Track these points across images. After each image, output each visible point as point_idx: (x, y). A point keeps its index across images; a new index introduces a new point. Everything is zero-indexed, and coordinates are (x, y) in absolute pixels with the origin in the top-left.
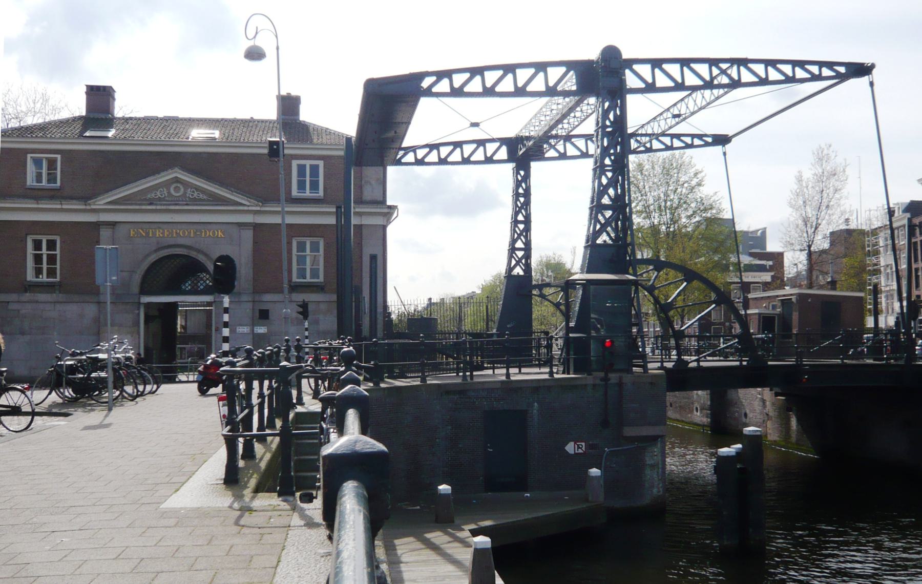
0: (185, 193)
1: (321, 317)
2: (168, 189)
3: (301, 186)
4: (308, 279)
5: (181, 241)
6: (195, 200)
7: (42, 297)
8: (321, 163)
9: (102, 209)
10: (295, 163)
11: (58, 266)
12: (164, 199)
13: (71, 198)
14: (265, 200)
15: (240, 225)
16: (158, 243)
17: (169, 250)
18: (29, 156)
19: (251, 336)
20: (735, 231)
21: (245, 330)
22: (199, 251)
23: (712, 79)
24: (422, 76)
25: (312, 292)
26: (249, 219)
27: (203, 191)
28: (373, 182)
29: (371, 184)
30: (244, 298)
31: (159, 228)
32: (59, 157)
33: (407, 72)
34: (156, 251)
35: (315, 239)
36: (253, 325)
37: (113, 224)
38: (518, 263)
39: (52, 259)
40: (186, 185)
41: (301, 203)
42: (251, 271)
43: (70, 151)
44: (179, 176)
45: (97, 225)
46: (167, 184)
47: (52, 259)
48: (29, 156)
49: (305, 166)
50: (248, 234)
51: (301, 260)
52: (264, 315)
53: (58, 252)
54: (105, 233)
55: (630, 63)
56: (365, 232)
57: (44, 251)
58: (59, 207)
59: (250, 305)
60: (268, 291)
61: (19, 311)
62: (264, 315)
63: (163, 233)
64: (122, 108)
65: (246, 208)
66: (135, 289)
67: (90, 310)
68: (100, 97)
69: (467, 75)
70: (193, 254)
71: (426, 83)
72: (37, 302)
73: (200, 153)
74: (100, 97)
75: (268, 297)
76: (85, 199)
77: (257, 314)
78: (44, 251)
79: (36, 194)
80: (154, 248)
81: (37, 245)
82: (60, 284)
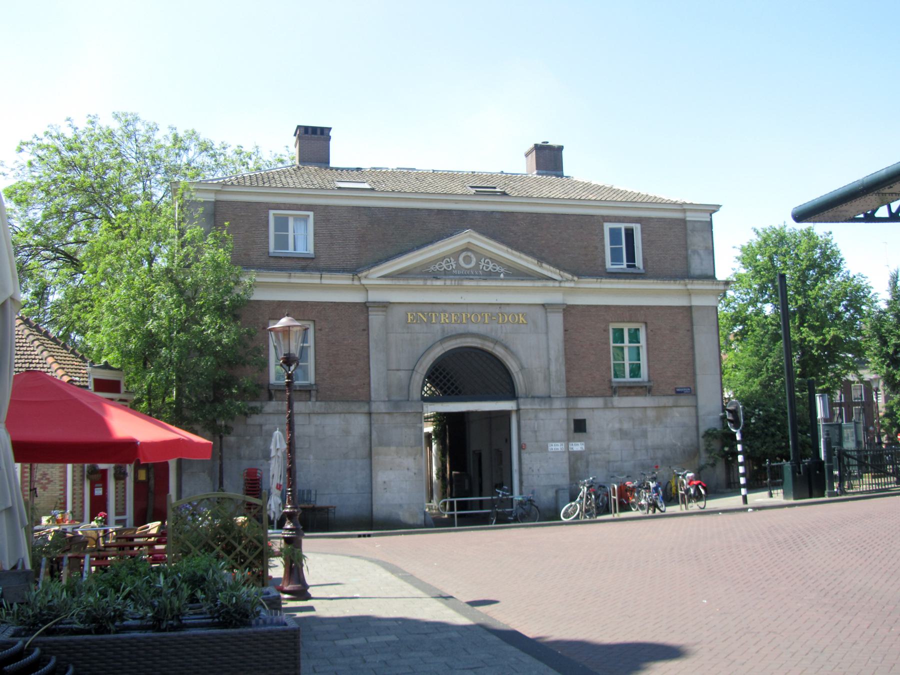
0: (478, 264)
1: (649, 427)
2: (457, 260)
4: (627, 378)
5: (473, 328)
9: (377, 284)
10: (607, 226)
11: (612, 362)
13: (330, 270)
14: (579, 273)
16: (443, 331)
17: (458, 341)
18: (272, 212)
19: (566, 455)
20: (269, 384)
21: (558, 447)
22: (496, 342)
25: (637, 394)
26: (556, 298)
28: (701, 252)
29: (699, 254)
30: (557, 404)
31: (444, 312)
32: (311, 214)
35: (634, 326)
36: (569, 440)
37: (385, 306)
40: (480, 255)
41: (635, 278)
42: (563, 369)
45: (365, 307)
46: (456, 254)
48: (272, 212)
50: (557, 320)
54: (376, 319)
56: (695, 315)
58: (317, 281)
59: (563, 414)
60: (583, 395)
61: (261, 426)
62: (580, 426)
63: (450, 318)
64: (340, 155)
65: (557, 284)
67: (359, 423)
68: (314, 141)
70: (489, 346)
73: (492, 212)
74: (314, 141)
76: (354, 270)
77: (572, 426)
79: (304, 264)
80: (439, 338)
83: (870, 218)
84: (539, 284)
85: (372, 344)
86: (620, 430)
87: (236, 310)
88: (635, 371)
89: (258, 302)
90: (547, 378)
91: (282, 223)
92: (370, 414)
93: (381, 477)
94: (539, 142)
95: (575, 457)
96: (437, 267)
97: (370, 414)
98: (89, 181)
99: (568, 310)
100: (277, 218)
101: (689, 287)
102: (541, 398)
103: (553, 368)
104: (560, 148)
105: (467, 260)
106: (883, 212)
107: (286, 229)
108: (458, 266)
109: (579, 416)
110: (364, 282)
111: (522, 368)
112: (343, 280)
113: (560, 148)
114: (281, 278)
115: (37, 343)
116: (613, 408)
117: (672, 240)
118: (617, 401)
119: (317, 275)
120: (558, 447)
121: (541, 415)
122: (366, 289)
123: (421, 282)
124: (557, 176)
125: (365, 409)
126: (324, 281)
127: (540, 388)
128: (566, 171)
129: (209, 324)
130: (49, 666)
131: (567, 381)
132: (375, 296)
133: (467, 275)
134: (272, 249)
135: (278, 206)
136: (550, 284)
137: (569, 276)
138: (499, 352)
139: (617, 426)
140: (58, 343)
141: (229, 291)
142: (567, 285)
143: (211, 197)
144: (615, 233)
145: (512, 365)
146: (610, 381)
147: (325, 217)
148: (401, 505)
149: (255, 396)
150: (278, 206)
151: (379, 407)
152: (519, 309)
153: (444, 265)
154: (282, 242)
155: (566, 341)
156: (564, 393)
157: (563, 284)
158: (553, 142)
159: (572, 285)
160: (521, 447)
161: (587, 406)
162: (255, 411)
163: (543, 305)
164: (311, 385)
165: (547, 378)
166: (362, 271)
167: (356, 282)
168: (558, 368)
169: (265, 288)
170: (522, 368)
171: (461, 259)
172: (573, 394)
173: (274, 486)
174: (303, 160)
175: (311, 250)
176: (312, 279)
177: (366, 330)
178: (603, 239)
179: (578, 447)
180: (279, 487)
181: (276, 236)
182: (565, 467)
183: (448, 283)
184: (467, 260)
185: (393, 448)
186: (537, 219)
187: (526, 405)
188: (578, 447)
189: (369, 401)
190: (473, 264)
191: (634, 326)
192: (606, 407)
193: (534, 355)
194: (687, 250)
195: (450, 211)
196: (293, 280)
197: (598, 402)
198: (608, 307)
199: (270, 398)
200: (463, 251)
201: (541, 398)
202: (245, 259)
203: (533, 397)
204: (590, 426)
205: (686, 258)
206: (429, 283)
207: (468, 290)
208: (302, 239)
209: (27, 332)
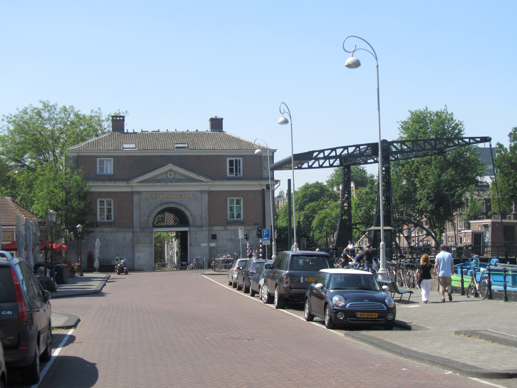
2: (166, 175)
3: (231, 171)
4: (235, 218)
5: (172, 200)
6: (179, 179)
7: (106, 229)
8: (241, 159)
9: (135, 185)
10: (228, 160)
12: (164, 180)
15: (201, 192)
18: (98, 159)
21: (205, 245)
22: (181, 205)
23: (424, 144)
24: (314, 152)
26: (206, 188)
27: (183, 175)
30: (205, 229)
32: (112, 159)
33: (307, 151)
34: (161, 205)
35: (238, 198)
37: (139, 193)
38: (345, 201)
39: (109, 210)
40: (175, 173)
43: (118, 156)
44: (172, 168)
45: (132, 193)
46: (166, 173)
47: (109, 210)
48: (98, 159)
49: (233, 161)
50: (206, 197)
51: (232, 209)
52: (214, 237)
53: (112, 207)
54: (136, 197)
55: (392, 143)
57: (105, 206)
58: (114, 184)
59: (207, 232)
62: (214, 237)
63: (164, 196)
64: (129, 127)
65: (205, 183)
66: (151, 225)
67: (129, 236)
69: (330, 151)
70: (179, 207)
71: (315, 154)
72: (103, 232)
75: (216, 228)
76: (127, 180)
77: (211, 237)
78: (105, 206)
81: (102, 202)
82: (421, 253)
83: (357, 146)
84: (198, 183)
85: (134, 207)
86: (230, 239)
87: (85, 196)
88: (239, 216)
89: (93, 192)
90: (201, 219)
91: (102, 163)
92: (133, 232)
93: (137, 255)
94: (213, 117)
95: (211, 249)
96: (162, 177)
97: (133, 232)
98: (34, 136)
99: (210, 193)
100: (100, 161)
101: (260, 183)
102: (198, 226)
103: (203, 215)
104: (222, 119)
105: (171, 175)
106: (351, 150)
107: (103, 165)
108: (167, 177)
109: (214, 233)
110: (131, 184)
111: (191, 215)
112: (124, 184)
113: (222, 119)
114: (101, 184)
115: (18, 209)
116: (227, 230)
117: (256, 165)
118: (229, 227)
119: (114, 182)
120: (205, 245)
121: (198, 233)
122: (132, 187)
123: (152, 184)
124: (219, 132)
125: (132, 230)
126: (117, 184)
127: (198, 222)
128: (224, 129)
129: (75, 203)
130: (276, 296)
131: (209, 220)
132: (135, 189)
133: (170, 181)
134: (98, 172)
135: (100, 157)
136: (202, 183)
137: (210, 180)
138: (183, 209)
139: (229, 237)
140: (24, 208)
141: (82, 189)
142: (209, 183)
143: (76, 155)
144: (231, 162)
145: (188, 214)
146: (227, 220)
147: (118, 160)
148: (144, 265)
149: (92, 227)
150: (100, 157)
151: (137, 229)
152: (192, 192)
153: (162, 177)
154: (102, 169)
155: (209, 204)
156: (208, 224)
157: (208, 183)
158: (219, 117)
159: (211, 183)
160: (191, 245)
161: (217, 229)
162: (91, 232)
163: (200, 191)
164: (112, 222)
165: (201, 219)
166: (130, 180)
167: (128, 185)
168: (205, 215)
169: (95, 187)
170: (191, 215)
171: (168, 175)
172: (210, 225)
173: (96, 257)
174: (114, 130)
175: (112, 173)
176: (113, 184)
177: (132, 201)
178: (226, 165)
179: (213, 245)
180: (98, 258)
181: (100, 168)
182: (207, 251)
183: (162, 184)
184: (171, 175)
185: (142, 245)
186: (199, 158)
187: (193, 229)
188: (213, 245)
189: (133, 227)
190: (173, 176)
191: (238, 198)
192: (225, 230)
193: (197, 209)
194: (261, 167)
195: (164, 156)
196: (105, 184)
197: (222, 228)
198: (227, 191)
199: (98, 226)
200: (169, 171)
201: (198, 226)
202: (86, 178)
203: (195, 226)
204: (218, 237)
205: (261, 172)
206: (155, 184)
207: (171, 186)
208: (109, 168)
209: (14, 205)
